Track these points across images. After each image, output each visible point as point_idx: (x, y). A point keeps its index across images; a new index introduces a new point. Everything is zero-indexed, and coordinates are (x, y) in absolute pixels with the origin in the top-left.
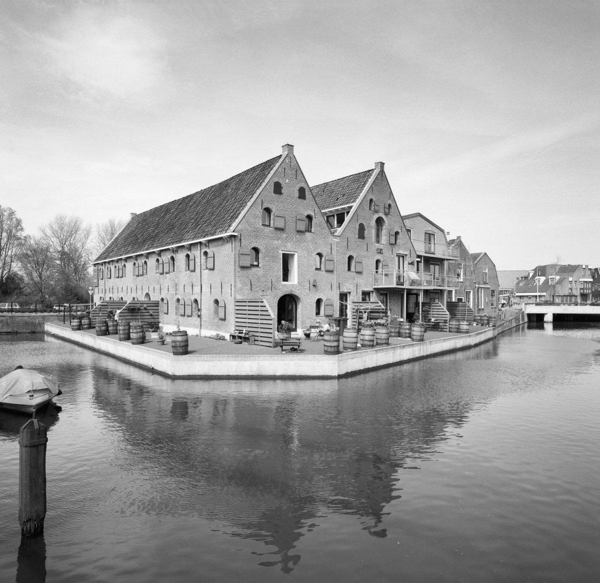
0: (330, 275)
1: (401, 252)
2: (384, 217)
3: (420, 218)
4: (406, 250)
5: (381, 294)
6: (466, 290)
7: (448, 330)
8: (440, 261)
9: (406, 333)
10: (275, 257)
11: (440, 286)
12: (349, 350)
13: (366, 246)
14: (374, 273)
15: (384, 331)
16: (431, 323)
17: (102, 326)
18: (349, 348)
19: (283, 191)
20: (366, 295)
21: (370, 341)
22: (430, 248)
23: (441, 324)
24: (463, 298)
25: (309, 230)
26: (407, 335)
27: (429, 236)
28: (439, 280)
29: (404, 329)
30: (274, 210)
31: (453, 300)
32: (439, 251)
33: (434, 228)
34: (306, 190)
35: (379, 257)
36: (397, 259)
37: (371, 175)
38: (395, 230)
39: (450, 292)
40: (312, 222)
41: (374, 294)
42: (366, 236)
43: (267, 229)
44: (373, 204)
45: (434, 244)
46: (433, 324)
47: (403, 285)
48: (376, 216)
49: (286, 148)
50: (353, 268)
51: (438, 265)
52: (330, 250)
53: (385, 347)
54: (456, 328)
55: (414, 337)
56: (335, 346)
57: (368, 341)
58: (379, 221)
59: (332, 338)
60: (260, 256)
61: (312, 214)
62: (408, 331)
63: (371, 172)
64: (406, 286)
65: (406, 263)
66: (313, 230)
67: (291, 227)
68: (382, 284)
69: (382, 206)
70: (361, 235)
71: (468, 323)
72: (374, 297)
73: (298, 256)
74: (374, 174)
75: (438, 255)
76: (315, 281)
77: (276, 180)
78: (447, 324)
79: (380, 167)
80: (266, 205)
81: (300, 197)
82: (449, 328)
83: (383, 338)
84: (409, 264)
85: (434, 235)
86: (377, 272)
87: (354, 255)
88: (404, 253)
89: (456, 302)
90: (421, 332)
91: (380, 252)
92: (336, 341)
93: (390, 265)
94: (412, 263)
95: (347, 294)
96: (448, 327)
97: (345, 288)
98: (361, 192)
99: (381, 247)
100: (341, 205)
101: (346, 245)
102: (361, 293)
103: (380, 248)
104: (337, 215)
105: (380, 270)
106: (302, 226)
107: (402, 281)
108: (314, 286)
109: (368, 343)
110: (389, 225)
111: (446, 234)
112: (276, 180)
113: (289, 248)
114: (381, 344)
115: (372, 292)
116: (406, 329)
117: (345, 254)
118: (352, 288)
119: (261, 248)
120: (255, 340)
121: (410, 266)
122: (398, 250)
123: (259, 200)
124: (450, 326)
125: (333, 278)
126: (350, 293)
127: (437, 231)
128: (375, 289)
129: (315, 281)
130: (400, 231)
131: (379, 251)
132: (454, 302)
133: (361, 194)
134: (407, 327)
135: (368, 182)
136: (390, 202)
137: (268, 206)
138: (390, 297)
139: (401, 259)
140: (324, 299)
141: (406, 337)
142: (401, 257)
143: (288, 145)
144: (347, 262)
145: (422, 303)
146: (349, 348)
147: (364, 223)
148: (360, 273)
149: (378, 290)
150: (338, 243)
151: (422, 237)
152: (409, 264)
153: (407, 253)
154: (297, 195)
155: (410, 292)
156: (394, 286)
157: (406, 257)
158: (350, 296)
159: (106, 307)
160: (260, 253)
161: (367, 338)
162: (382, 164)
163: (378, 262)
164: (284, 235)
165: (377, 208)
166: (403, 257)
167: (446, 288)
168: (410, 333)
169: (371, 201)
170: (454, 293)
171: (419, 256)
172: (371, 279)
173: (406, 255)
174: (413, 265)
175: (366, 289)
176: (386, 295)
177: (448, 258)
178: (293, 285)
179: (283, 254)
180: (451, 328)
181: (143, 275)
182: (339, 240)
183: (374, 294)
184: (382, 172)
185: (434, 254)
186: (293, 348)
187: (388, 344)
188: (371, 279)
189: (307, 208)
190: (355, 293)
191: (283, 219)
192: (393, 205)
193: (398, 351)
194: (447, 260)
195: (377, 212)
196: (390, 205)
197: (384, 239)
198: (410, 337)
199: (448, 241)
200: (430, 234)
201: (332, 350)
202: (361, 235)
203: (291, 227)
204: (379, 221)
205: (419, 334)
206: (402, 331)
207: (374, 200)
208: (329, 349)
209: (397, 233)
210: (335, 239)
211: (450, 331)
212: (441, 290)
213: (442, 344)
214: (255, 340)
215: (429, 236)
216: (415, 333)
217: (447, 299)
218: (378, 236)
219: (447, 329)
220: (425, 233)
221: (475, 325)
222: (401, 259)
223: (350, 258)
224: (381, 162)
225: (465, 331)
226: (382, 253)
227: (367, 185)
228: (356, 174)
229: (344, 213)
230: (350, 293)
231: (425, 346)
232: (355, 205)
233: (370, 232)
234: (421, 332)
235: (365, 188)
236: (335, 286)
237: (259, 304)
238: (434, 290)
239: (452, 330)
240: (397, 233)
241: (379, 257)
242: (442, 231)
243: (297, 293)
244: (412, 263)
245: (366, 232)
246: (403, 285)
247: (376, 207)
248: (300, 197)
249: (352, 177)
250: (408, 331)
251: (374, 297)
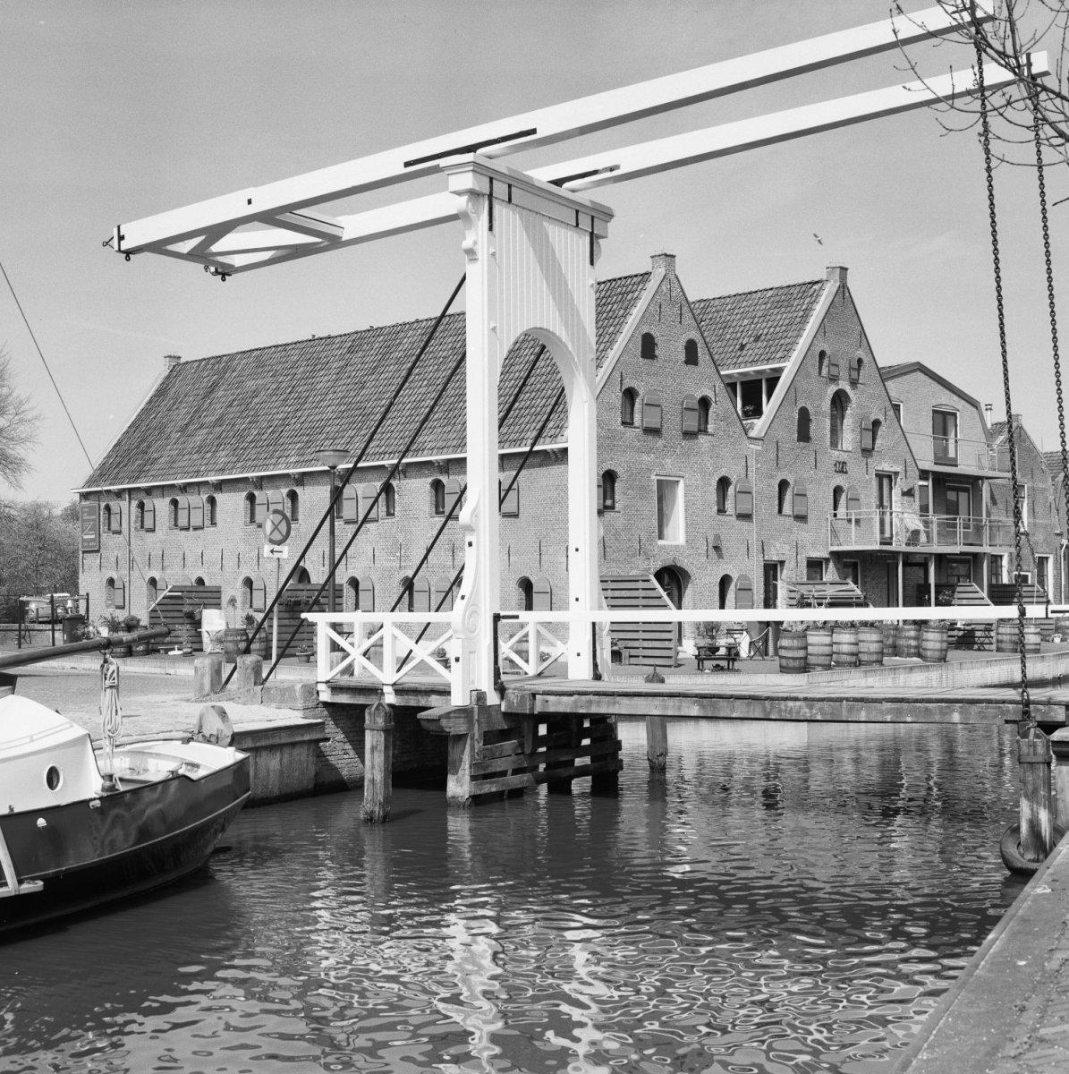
0: (744, 525)
1: (886, 467)
2: (848, 388)
3: (919, 373)
4: (895, 462)
5: (846, 565)
6: (1037, 555)
7: (994, 647)
8: (971, 484)
9: (909, 647)
10: (644, 489)
11: (971, 545)
12: (819, 668)
13: (812, 458)
14: (830, 517)
15: (875, 637)
16: (955, 633)
17: (241, 641)
18: (818, 665)
19: (657, 352)
20: (815, 566)
21: (852, 654)
22: (946, 450)
23: (978, 634)
24: (1029, 574)
25: (703, 430)
26: (913, 651)
27: (943, 421)
28: (969, 528)
29: (905, 637)
30: (641, 392)
31: (1005, 580)
32: (970, 457)
33: (955, 398)
34: (699, 345)
35: (839, 480)
36: (875, 483)
37: (815, 298)
38: (873, 418)
39: (996, 560)
40: (707, 411)
41: (831, 565)
42: (812, 434)
43: (630, 432)
44: (826, 362)
45: (956, 441)
46: (961, 633)
47: (891, 544)
48: (832, 389)
49: (661, 262)
50: (787, 509)
51: (966, 490)
52: (743, 472)
53: (875, 666)
54: (1011, 642)
55: (929, 653)
56: (801, 658)
57: (847, 654)
58: (840, 401)
59: (796, 643)
60: (616, 489)
61: (711, 394)
62: (913, 643)
63: (816, 287)
64: (899, 545)
65: (896, 492)
66: (711, 427)
67: (672, 426)
68: (849, 543)
69: (843, 364)
70: (804, 435)
71: (1038, 630)
72: (830, 573)
73: (686, 486)
74: (825, 293)
75: (966, 467)
76: (717, 537)
77: (645, 330)
78: (993, 634)
79: (838, 278)
80: (628, 383)
81: (687, 362)
82: (998, 641)
83: (872, 650)
84: (904, 494)
85: (955, 415)
86: (835, 515)
87: (791, 480)
88: (893, 470)
89: (1014, 586)
90: (942, 641)
91: (841, 468)
92: (801, 648)
93: (862, 497)
94: (909, 493)
95: (775, 566)
96: (994, 640)
97: (773, 551)
98: (799, 336)
99: (844, 457)
100: (753, 362)
101: (773, 456)
102: (805, 564)
103: (841, 459)
104: (742, 383)
105: (842, 511)
106: (692, 424)
107: (887, 535)
108: (717, 548)
109: (849, 659)
110: (860, 406)
111: (983, 408)
112: (645, 331)
113: (670, 465)
114: (869, 663)
115: (827, 560)
116: (910, 638)
117: (772, 477)
118: (787, 553)
119: (619, 470)
120: (630, 656)
121: (905, 498)
122: (880, 463)
123: (617, 375)
124: (1000, 637)
125: (750, 530)
126: (782, 563)
127: (960, 404)
128: (832, 553)
129: (717, 537)
130: (882, 419)
131: (839, 467)
132: (1005, 585)
133: (801, 341)
134: (912, 633)
135: (815, 313)
136: (860, 353)
137: (632, 385)
138: (863, 571)
139: (885, 481)
140: (735, 576)
141: (909, 655)
142: (885, 478)
143: (666, 255)
144: (777, 494)
145: (936, 586)
146: (818, 665)
147: (809, 407)
148: (801, 518)
149: (837, 556)
150: (759, 454)
151: (927, 425)
152: (904, 494)
153: (898, 469)
154: (683, 357)
155: (909, 560)
156: (877, 547)
157: (896, 479)
158: (782, 570)
159: (180, 602)
160: (618, 480)
161: (846, 648)
162: (844, 270)
163: (838, 491)
164: (660, 442)
165: (834, 371)
166: (889, 477)
167: (986, 549)
168: (917, 647)
169: (822, 354)
170: (1005, 562)
171: (924, 474)
172: (825, 532)
173: (896, 473)
174: (913, 495)
175: (815, 554)
176: (855, 566)
177: (991, 474)
178: (677, 547)
179: (1001, 556)
180: (1001, 642)
181: (202, 528)
182: (760, 448)
183: (831, 565)
184: (843, 289)
185: (956, 466)
186: (718, 666)
187: (880, 662)
188: (824, 531)
189: (702, 382)
190: (793, 564)
191: (659, 409)
192: (866, 360)
193: (902, 677)
194: (988, 478)
195: (833, 379)
196: (860, 361)
197: (849, 439)
198: (919, 655)
199: (989, 426)
200: (945, 414)
201: (797, 664)
202: (804, 435)
203: (672, 426)
204: (840, 401)
205: (938, 646)
206: (902, 642)
207: (828, 352)
208: (791, 664)
209: (876, 424)
210: (752, 446)
211: (999, 650)
212: (975, 555)
213: (982, 670)
214: (630, 656)
215: (943, 421)
216: (930, 645)
217: (989, 580)
218: (835, 431)
219: (991, 644)
220: (934, 412)
221: (1057, 640)
222: (885, 481)
223: (783, 485)
224: (841, 268)
225: (1033, 647)
226: (846, 473)
227: (812, 320)
228: (782, 288)
229: (760, 381)
230: (782, 563)
231: (950, 673)
232: (789, 368)
233: (821, 426)
234: (942, 641)
235: (808, 327)
236: (755, 548)
237: (640, 585)
238: (962, 554)
239: (1004, 646)
240: (876, 424)
241: (839, 480)
242: (974, 403)
243: (684, 563)
244: (909, 493)
245: (813, 427)
246: (891, 544)
247: (832, 368)
248: (687, 362)
249: (770, 293)
250: (913, 643)
251: (830, 573)
